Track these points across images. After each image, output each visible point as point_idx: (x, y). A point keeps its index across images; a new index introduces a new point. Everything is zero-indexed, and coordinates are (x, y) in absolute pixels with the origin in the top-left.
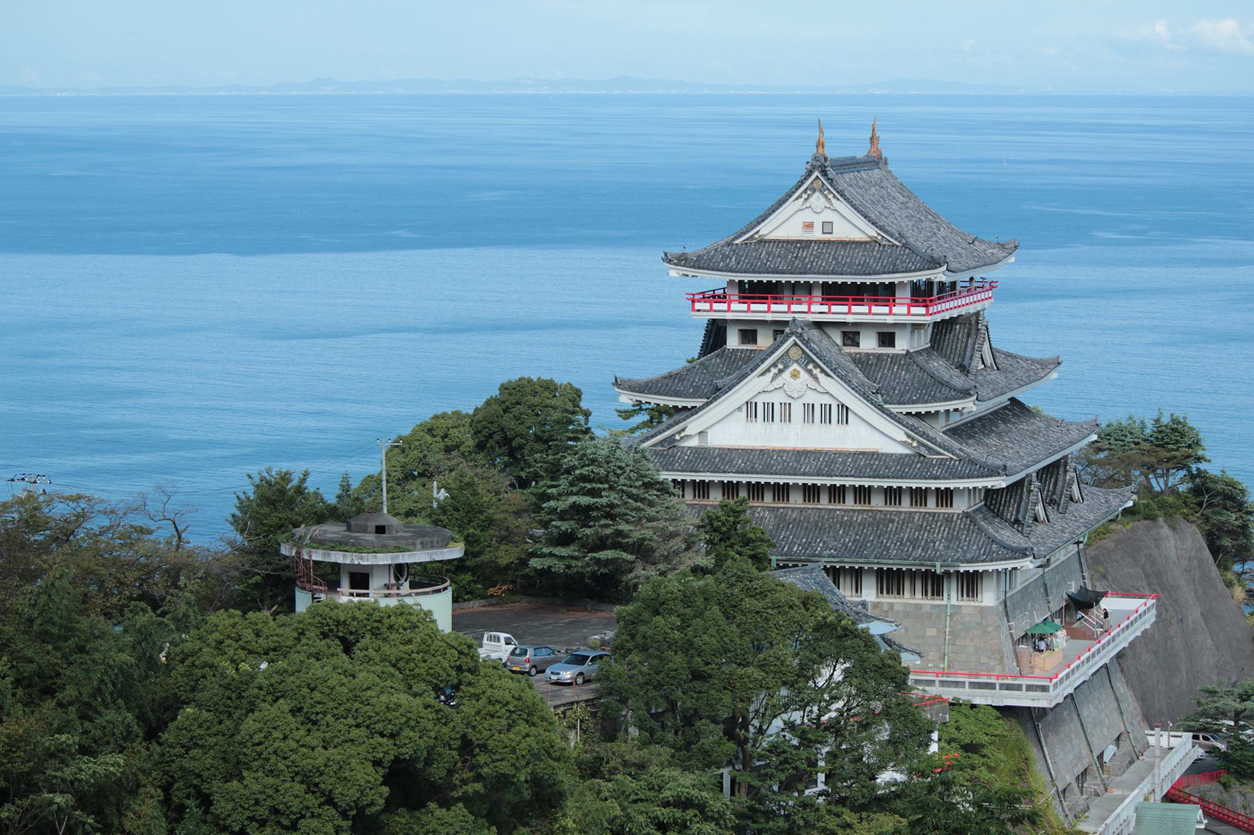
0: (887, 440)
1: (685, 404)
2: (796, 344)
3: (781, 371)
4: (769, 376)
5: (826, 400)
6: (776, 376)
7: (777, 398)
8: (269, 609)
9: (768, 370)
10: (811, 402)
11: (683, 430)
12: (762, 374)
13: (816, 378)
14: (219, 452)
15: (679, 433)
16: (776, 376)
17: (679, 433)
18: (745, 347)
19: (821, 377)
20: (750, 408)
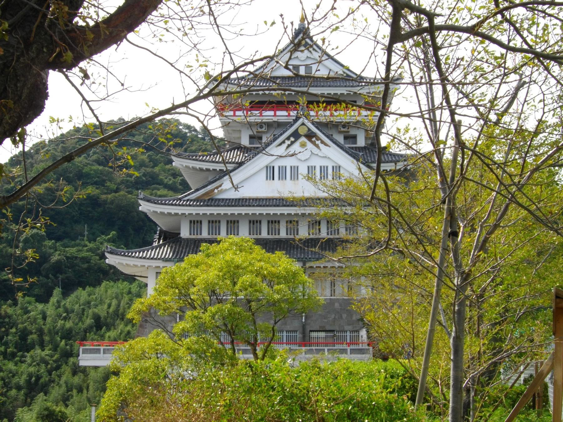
0: (139, 45)
1: (176, 212)
2: (303, 124)
3: (292, 143)
4: (284, 146)
5: (324, 163)
6: (289, 146)
7: (288, 163)
8: (34, 252)
9: (283, 142)
10: (313, 165)
11: (220, 186)
12: (280, 145)
13: (317, 146)
14: (429, 94)
15: (217, 188)
16: (289, 146)
17: (217, 188)
18: (251, 146)
19: (321, 146)
20: (270, 172)
